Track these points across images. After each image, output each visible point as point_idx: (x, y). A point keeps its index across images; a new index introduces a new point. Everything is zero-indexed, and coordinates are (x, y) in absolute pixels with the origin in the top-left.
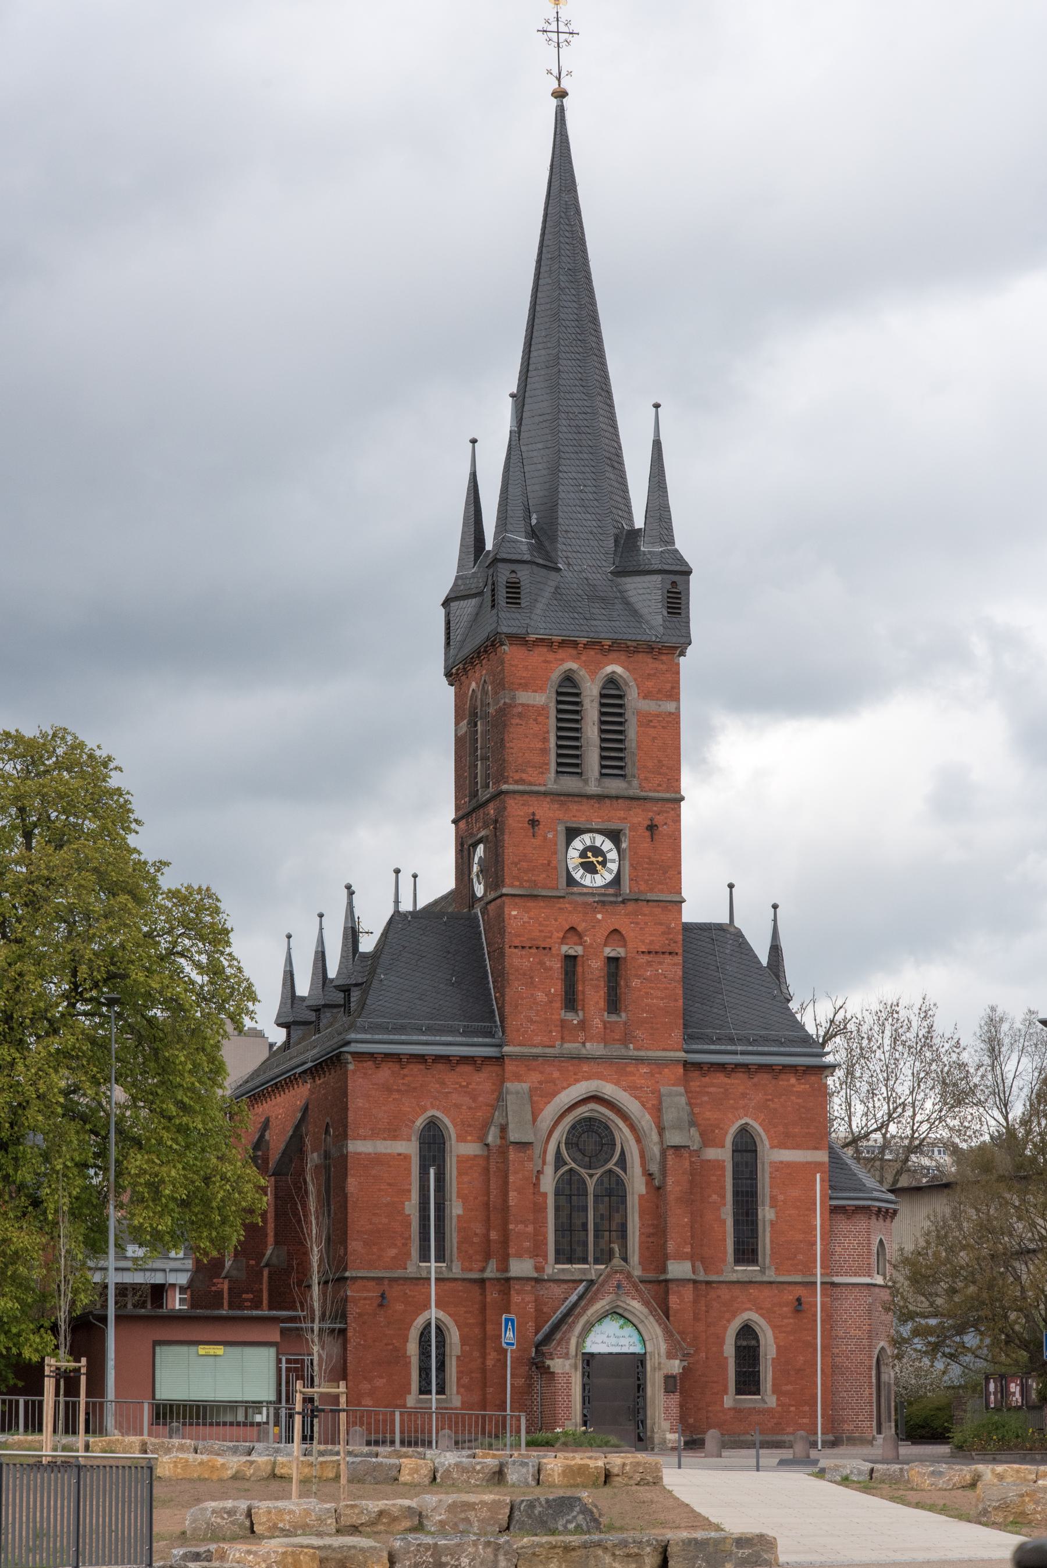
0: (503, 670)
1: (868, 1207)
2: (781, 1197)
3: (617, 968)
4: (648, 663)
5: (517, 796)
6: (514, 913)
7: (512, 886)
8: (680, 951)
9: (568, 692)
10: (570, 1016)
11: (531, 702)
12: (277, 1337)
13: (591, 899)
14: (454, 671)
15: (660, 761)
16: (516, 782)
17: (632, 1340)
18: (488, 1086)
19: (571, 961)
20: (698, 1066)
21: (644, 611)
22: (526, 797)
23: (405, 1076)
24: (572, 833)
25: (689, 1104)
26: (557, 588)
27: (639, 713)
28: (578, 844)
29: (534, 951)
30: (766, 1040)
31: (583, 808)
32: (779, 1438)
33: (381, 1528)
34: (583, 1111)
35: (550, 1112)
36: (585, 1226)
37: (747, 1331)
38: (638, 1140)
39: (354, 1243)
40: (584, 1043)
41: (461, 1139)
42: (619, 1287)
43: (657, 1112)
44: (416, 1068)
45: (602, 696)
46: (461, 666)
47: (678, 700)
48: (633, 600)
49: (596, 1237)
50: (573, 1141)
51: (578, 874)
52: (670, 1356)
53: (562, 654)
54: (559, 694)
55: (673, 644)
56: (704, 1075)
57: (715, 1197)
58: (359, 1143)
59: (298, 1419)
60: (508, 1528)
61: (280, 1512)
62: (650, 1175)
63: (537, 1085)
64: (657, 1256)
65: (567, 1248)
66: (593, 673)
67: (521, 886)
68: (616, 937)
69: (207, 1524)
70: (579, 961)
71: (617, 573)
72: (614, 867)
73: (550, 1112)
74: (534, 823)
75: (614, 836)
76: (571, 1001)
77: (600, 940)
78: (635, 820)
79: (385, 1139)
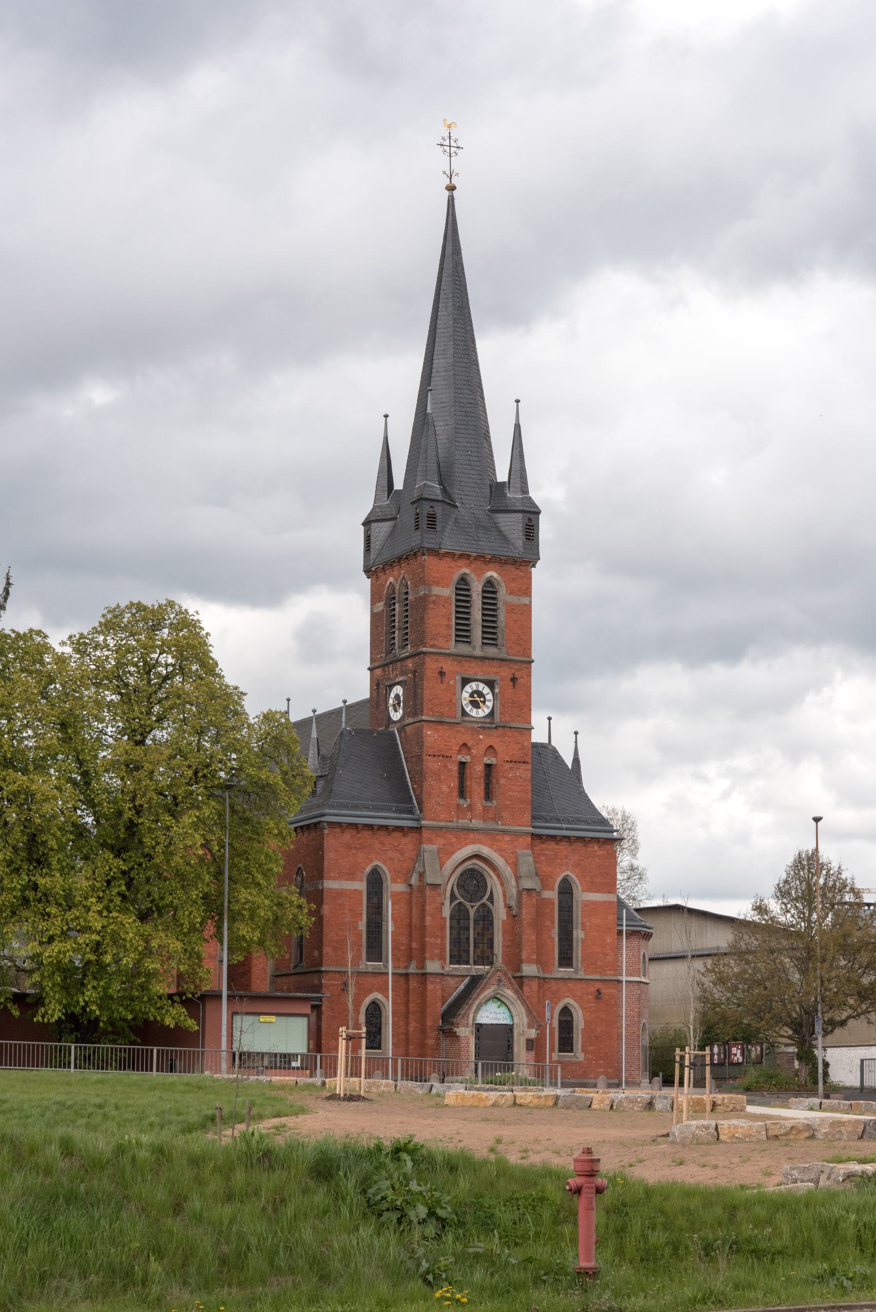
0: (423, 571)
1: (639, 932)
2: (588, 924)
3: (490, 771)
4: (513, 571)
5: (432, 656)
6: (429, 733)
7: (428, 715)
8: (530, 761)
9: (463, 586)
10: (461, 802)
11: (440, 594)
12: (308, 1010)
13: (476, 725)
14: (373, 569)
15: (519, 636)
16: (431, 646)
17: (505, 1016)
18: (410, 847)
19: (462, 764)
20: (540, 837)
21: (510, 537)
22: (437, 657)
23: (360, 838)
24: (465, 681)
25: (535, 862)
26: (456, 519)
27: (506, 604)
28: (468, 689)
29: (441, 758)
30: (579, 821)
31: (473, 665)
32: (585, 1081)
33: (792, 1137)
34: (468, 865)
35: (450, 864)
36: (468, 939)
37: (566, 1011)
38: (502, 885)
39: (327, 948)
40: (471, 820)
41: (394, 881)
42: (500, 981)
43: (515, 866)
44: (366, 834)
45: (484, 591)
46: (381, 566)
47: (530, 596)
48: (503, 529)
49: (475, 947)
50: (462, 884)
51: (468, 709)
52: (530, 1026)
53: (460, 562)
54: (457, 589)
55: (528, 557)
56: (405, 836)
57: (548, 923)
58: (330, 882)
59: (687, 1070)
60: (862, 1137)
61: (736, 1127)
62: (509, 908)
63: (442, 847)
64: (515, 962)
65: (457, 954)
66: (479, 577)
67: (433, 715)
68: (491, 751)
69: (694, 1135)
70: (468, 765)
71: (493, 511)
72: (490, 704)
73: (450, 864)
74: (442, 674)
75: (490, 684)
76: (462, 793)
77: (482, 753)
78: (504, 674)
79: (347, 880)
